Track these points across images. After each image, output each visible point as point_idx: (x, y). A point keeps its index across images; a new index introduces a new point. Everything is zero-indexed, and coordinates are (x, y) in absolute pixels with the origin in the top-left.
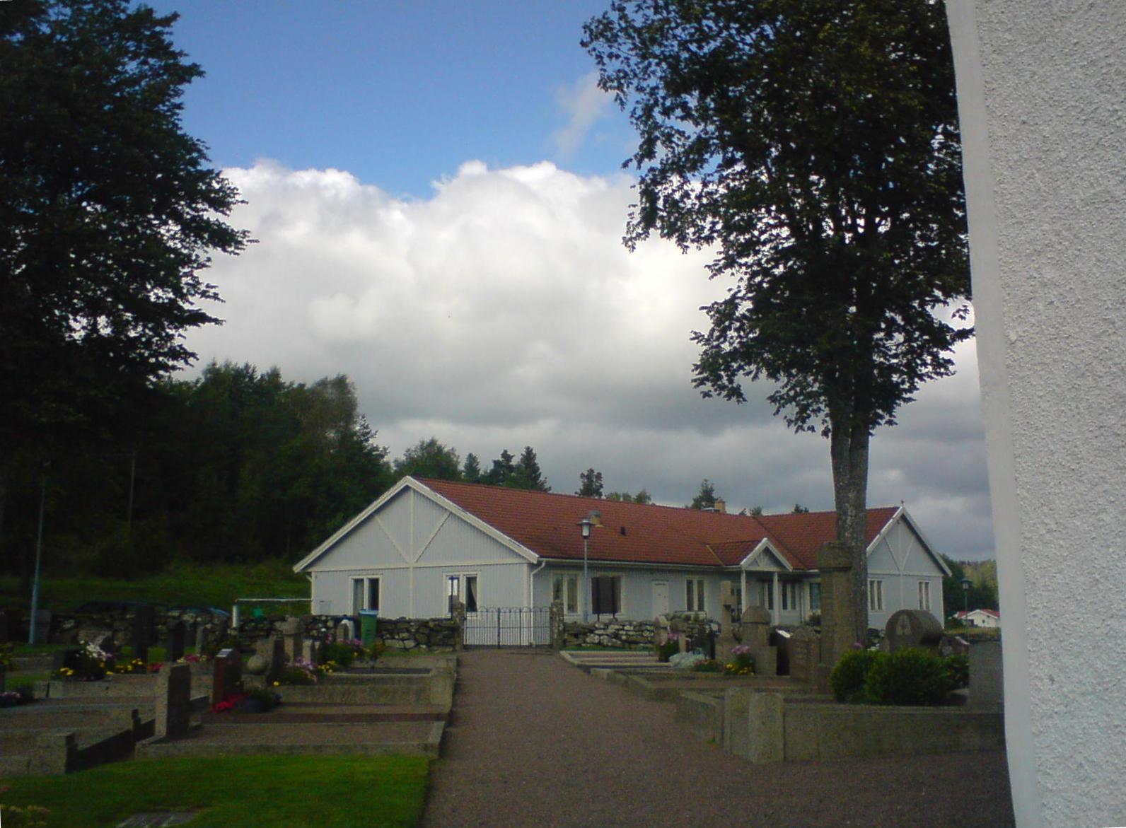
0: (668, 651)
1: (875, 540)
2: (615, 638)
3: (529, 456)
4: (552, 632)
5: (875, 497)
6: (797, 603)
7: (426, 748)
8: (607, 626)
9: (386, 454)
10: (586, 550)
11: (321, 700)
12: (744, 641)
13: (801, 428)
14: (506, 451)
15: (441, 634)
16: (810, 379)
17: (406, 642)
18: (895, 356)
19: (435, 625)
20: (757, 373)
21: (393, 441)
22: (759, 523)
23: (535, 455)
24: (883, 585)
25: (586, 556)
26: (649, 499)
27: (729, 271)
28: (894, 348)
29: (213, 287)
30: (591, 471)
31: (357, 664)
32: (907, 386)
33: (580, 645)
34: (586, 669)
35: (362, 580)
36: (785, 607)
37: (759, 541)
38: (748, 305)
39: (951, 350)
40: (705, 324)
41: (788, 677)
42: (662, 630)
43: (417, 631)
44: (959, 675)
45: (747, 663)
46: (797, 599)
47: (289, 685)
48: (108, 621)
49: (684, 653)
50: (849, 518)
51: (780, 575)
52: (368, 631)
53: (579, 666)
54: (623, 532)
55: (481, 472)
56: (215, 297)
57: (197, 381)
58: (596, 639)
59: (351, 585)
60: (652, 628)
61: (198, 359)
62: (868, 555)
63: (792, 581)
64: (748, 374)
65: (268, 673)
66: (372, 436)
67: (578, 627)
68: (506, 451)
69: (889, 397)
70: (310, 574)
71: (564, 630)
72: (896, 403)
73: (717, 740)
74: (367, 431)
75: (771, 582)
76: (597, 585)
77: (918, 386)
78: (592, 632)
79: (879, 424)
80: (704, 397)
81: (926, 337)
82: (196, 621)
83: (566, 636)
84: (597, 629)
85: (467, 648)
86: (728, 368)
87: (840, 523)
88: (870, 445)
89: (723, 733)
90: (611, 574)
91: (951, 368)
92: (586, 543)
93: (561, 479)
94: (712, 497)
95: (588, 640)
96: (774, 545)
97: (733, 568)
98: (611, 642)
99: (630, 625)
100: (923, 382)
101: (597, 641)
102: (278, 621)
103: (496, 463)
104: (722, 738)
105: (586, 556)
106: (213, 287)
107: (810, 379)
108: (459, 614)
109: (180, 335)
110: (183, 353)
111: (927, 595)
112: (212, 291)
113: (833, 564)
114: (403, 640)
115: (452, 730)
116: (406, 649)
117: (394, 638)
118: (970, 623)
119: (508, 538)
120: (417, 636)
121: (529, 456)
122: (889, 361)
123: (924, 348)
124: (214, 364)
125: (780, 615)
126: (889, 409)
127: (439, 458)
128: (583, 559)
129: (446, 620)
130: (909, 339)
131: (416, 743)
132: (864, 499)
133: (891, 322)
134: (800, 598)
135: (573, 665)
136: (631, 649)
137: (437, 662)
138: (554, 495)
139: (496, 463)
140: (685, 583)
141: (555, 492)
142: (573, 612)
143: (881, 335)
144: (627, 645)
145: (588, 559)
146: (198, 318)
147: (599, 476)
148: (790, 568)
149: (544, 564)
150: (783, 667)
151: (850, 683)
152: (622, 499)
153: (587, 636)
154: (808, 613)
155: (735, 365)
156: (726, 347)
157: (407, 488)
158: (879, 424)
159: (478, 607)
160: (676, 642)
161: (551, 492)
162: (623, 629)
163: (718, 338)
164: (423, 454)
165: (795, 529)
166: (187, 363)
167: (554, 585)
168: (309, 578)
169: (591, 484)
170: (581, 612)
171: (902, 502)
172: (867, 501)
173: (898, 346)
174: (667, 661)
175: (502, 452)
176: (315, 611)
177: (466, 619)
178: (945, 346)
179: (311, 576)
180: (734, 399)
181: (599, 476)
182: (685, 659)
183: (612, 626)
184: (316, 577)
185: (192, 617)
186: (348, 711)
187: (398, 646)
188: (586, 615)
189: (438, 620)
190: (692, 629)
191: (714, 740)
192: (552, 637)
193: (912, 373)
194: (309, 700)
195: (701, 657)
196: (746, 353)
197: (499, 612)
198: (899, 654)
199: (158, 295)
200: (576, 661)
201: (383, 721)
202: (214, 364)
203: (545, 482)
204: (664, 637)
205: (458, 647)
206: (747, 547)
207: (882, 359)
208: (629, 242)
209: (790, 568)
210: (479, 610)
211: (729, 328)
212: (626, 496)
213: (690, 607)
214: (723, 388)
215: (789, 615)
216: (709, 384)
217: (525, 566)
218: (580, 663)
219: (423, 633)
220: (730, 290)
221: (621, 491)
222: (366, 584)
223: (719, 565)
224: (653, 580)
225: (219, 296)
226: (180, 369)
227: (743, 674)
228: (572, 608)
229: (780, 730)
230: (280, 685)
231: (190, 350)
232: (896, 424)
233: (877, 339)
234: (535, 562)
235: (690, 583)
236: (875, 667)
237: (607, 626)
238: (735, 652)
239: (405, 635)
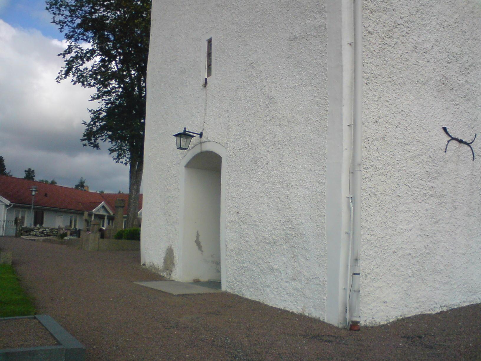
4: (17, 230)
8: (39, 229)
13: (117, 162)
16: (124, 144)
22: (102, 196)
30: (30, 169)
38: (105, 114)
40: (88, 117)
51: (108, 216)
54: (46, 195)
58: (35, 233)
64: (102, 140)
71: (22, 230)
78: (33, 230)
107: (124, 144)
147: (33, 171)
156: (95, 129)
163: (92, 125)
169: (30, 174)
180: (95, 148)
181: (33, 171)
192: (16, 232)
196: (102, 129)
206: (97, 204)
208: (58, 79)
209: (112, 214)
211: (97, 122)
212: (47, 182)
214: (92, 143)
216: (87, 141)
221: (45, 180)
235: (71, 217)
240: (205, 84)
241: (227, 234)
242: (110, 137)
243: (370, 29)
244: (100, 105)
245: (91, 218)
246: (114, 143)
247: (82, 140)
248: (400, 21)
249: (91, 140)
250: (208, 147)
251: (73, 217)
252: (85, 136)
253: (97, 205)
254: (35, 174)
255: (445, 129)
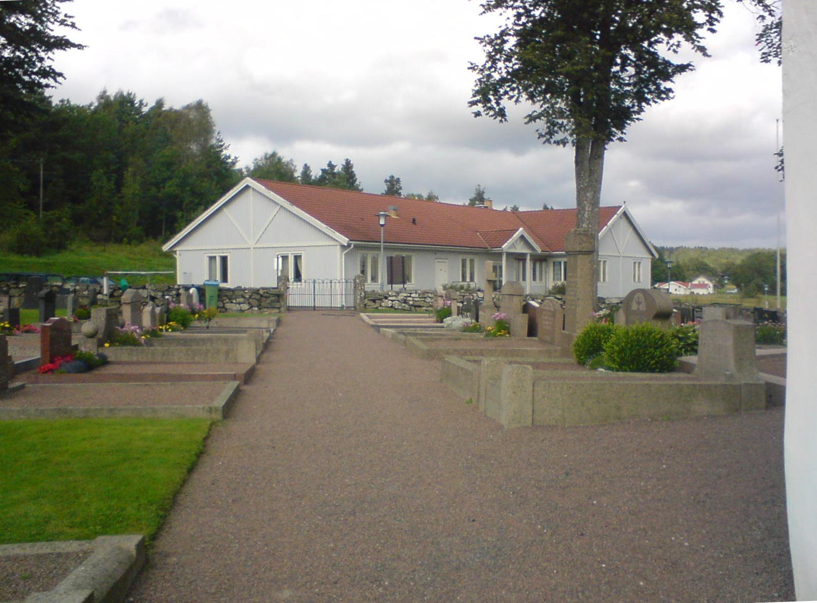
0: (444, 314)
1: (603, 230)
2: (404, 303)
3: (348, 166)
5: (607, 199)
6: (543, 278)
7: (210, 410)
8: (398, 294)
9: (236, 162)
10: (382, 235)
11: (145, 360)
12: (501, 309)
14: (330, 162)
15: (270, 299)
17: (242, 305)
18: (629, 85)
19: (264, 293)
20: (518, 97)
21: (243, 152)
23: (353, 165)
24: (607, 264)
25: (382, 238)
26: (437, 198)
27: (499, 10)
28: (628, 78)
29: (70, 17)
31: (196, 324)
32: (636, 108)
33: (377, 308)
34: (377, 328)
35: (215, 257)
36: (534, 279)
37: (518, 230)
39: (672, 81)
40: (480, 56)
41: (536, 338)
42: (440, 298)
43: (250, 297)
44: (682, 343)
45: (504, 327)
46: (544, 273)
47: (118, 346)
48: (5, 289)
49: (455, 316)
50: (586, 212)
52: (211, 297)
53: (373, 326)
54: (414, 221)
55: (313, 178)
56: (73, 25)
57: (91, 105)
59: (207, 260)
60: (432, 296)
61: (65, 79)
62: (599, 238)
63: (540, 260)
64: (511, 98)
65: (100, 336)
66: (225, 148)
67: (376, 294)
68: (330, 162)
69: (622, 117)
70: (175, 252)
72: (626, 123)
73: (474, 401)
74: (222, 143)
75: (524, 260)
76: (391, 261)
77: (645, 109)
78: (386, 298)
79: (612, 140)
80: (476, 117)
81: (652, 70)
82: (75, 289)
83: (366, 301)
84: (390, 296)
85: (289, 309)
86: (496, 92)
87: (579, 216)
88: (605, 155)
89: (479, 397)
90: (404, 254)
91: (671, 95)
92: (382, 231)
93: (370, 181)
94: (483, 198)
95: (383, 304)
96: (528, 233)
97: (497, 250)
98: (401, 306)
99: (416, 293)
100: (649, 106)
101: (390, 305)
102: (140, 288)
103: (324, 171)
104: (478, 400)
105: (382, 238)
106: (70, 17)
108: (283, 283)
109: (48, 58)
110: (51, 73)
111: (639, 270)
112: (69, 21)
113: (578, 249)
114: (239, 303)
115: (245, 387)
116: (242, 311)
117: (232, 302)
118: (666, 291)
119: (325, 226)
120: (250, 300)
121: (348, 166)
122: (623, 88)
123: (650, 79)
124: (105, 92)
125: (531, 285)
126: (621, 127)
127: (278, 166)
128: (380, 242)
129: (273, 288)
130: (638, 73)
131: (201, 406)
132: (599, 198)
133: (625, 58)
134: (546, 272)
135: (368, 324)
136: (416, 312)
137: (262, 322)
138: (365, 194)
139: (324, 171)
140: (461, 260)
141: (366, 192)
142: (375, 282)
143: (618, 68)
144: (413, 308)
145: (384, 242)
146: (63, 44)
147: (398, 181)
148: (539, 251)
149: (352, 246)
150: (532, 331)
151: (590, 350)
152: (417, 198)
153: (383, 302)
154: (551, 285)
155: (502, 91)
156: (496, 76)
157: (247, 187)
158: (612, 140)
159: (303, 277)
160: (450, 307)
161: (363, 192)
162: (410, 297)
163: (490, 68)
164: (267, 162)
165: (543, 222)
166: (56, 81)
167: (361, 261)
168: (175, 256)
169: (393, 186)
170: (379, 285)
171: (625, 202)
172: (601, 200)
173: (630, 77)
174: (442, 322)
175: (328, 163)
176: (180, 281)
177: (288, 288)
178: (667, 77)
179: (176, 254)
181: (398, 181)
182: (456, 321)
183: (402, 294)
184: (180, 255)
185: (72, 286)
186: (160, 369)
187: (235, 309)
188: (382, 285)
189: (266, 289)
190: (464, 296)
191: (471, 401)
193: (640, 98)
194: (135, 359)
195: (468, 320)
197: (314, 282)
198: (634, 327)
199: (24, 21)
200: (371, 322)
201: (187, 380)
202: (105, 92)
203: (359, 185)
204: (440, 303)
205: (282, 309)
207: (617, 87)
209: (539, 251)
210: (303, 281)
212: (420, 196)
213: (464, 279)
214: (491, 108)
215: (537, 285)
217: (339, 247)
218: (374, 323)
219: (255, 299)
220: (500, 27)
222: (218, 260)
223: (486, 248)
224: (436, 259)
225: (76, 26)
226: (53, 87)
227: (500, 335)
228: (374, 279)
229: (530, 398)
230: (110, 346)
231: (57, 70)
232: (625, 141)
233: (614, 72)
234: (346, 244)
235: (464, 262)
236: (614, 339)
237: (398, 294)
238: (495, 318)
239: (242, 300)
247: (473, 103)
249: (489, 101)
251: (468, 258)
252: (477, 93)
254: (402, 184)
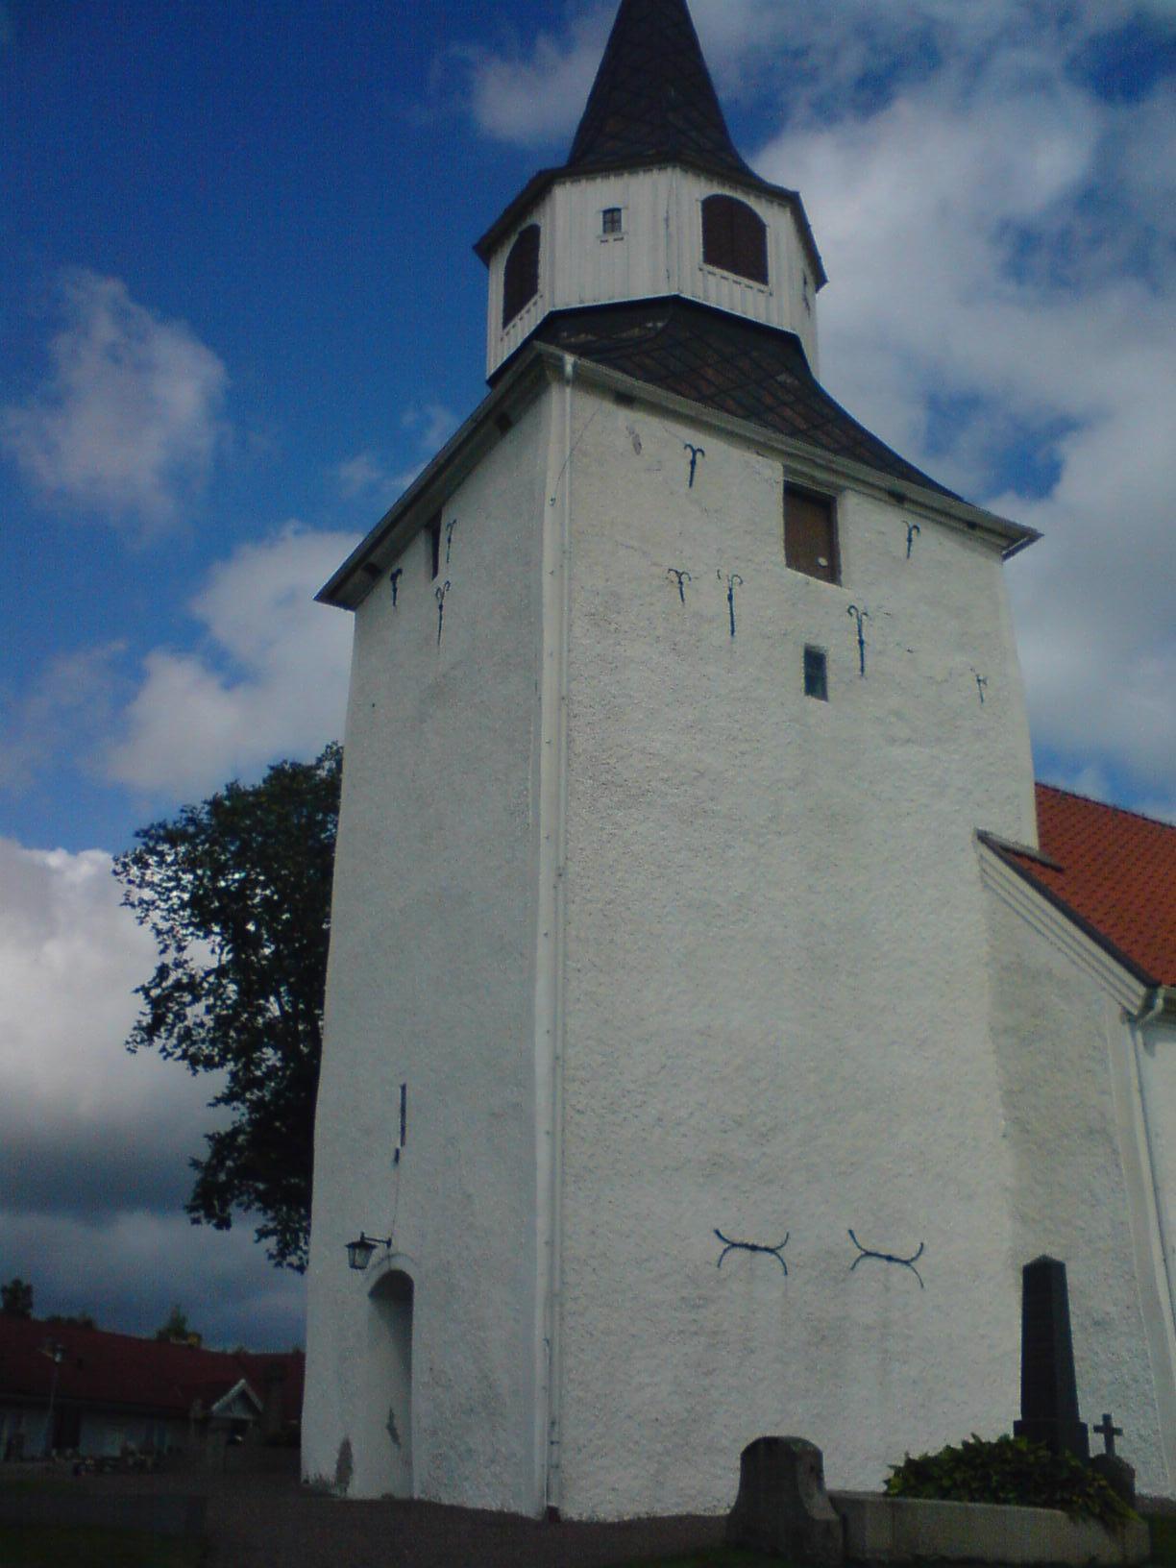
13: (279, 1264)
30: (17, 1283)
147: (28, 1290)
240: (397, 1158)
241: (421, 1405)
242: (261, 1196)
243: (579, 1107)
244: (236, 1116)
245: (575, 366)
246: (270, 1214)
248: (632, 1087)
250: (399, 1264)
253: (226, 1391)
255: (717, 1233)
